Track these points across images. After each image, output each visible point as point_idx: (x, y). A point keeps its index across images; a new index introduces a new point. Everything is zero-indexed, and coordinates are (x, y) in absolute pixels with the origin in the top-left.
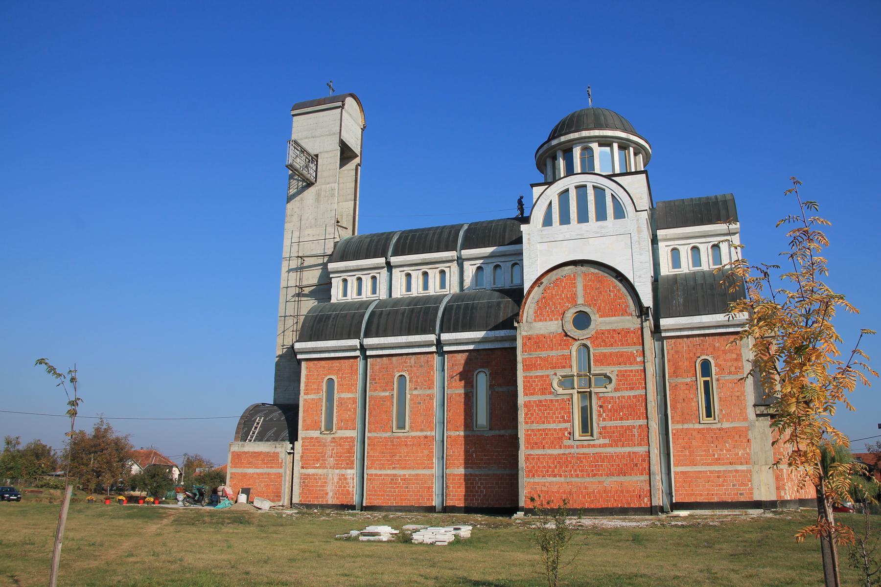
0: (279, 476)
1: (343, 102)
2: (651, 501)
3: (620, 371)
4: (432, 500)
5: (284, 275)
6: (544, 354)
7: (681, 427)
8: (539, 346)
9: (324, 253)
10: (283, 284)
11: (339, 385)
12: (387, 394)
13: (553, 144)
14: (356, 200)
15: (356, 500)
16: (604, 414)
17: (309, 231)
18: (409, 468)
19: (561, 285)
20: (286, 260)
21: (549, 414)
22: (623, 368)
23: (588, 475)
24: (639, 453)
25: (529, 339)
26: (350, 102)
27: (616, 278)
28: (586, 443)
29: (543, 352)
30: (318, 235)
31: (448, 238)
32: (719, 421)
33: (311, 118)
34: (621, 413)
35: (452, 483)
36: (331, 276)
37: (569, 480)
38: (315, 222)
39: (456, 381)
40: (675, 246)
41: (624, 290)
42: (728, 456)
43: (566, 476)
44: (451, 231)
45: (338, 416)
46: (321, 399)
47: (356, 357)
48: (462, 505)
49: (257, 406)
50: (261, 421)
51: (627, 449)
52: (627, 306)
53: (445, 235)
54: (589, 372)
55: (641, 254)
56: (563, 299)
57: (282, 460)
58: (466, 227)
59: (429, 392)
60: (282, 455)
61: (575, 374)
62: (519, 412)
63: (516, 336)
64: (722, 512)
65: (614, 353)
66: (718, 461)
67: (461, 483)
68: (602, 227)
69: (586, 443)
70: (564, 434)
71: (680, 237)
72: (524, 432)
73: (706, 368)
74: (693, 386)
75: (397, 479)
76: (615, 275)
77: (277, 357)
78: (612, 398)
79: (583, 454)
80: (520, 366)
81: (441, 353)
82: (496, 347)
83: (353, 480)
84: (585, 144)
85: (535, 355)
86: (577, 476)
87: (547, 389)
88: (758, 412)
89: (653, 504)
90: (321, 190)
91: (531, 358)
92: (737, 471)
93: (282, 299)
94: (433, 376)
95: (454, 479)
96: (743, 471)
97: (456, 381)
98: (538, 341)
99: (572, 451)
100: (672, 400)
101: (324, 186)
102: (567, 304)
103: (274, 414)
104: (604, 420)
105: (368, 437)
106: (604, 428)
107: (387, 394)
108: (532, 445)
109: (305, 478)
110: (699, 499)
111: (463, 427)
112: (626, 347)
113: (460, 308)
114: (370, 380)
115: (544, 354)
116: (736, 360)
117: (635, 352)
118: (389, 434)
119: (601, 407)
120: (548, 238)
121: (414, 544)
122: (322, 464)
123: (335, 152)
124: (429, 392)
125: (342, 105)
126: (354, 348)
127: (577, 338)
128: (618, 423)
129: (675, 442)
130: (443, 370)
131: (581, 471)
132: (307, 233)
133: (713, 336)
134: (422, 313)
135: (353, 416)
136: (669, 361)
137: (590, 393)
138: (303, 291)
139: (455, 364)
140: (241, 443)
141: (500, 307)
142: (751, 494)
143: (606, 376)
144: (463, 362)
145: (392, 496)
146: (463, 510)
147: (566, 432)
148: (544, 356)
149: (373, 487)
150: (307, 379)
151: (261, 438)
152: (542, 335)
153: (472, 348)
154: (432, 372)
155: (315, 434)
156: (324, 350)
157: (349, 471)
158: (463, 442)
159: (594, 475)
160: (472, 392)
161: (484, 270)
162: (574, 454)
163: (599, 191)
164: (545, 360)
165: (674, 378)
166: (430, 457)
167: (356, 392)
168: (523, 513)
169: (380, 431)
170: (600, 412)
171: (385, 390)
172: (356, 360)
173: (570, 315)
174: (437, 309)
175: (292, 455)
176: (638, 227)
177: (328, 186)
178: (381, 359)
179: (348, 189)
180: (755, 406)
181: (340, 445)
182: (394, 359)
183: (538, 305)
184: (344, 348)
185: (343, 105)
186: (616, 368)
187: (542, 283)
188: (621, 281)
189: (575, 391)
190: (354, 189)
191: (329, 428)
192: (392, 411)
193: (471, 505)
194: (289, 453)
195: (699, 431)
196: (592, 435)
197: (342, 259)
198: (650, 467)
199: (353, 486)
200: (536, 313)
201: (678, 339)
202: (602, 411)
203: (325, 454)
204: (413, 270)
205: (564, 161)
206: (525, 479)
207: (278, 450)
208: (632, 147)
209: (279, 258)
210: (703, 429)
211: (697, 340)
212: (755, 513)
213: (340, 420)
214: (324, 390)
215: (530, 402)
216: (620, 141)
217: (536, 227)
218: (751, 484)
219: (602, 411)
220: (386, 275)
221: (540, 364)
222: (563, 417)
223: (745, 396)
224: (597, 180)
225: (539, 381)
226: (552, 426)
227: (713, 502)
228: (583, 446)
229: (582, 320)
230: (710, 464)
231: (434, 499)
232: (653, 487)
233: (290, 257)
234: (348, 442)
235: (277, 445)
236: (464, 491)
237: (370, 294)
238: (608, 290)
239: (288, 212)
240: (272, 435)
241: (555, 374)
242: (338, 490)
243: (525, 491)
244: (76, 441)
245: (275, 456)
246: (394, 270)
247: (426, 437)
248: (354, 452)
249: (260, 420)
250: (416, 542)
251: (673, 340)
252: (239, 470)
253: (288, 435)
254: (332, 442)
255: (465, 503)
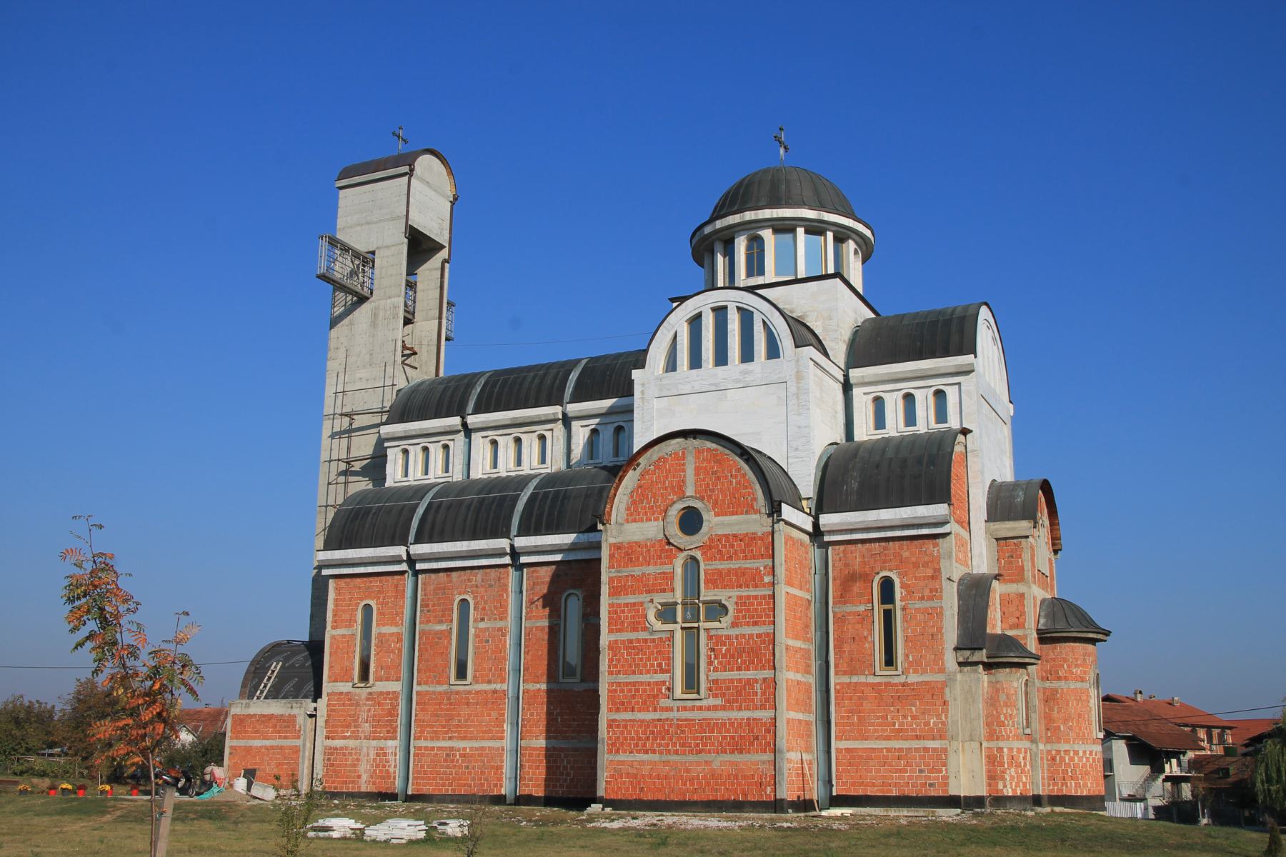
0: (296, 750)
1: (410, 165)
2: (775, 792)
3: (739, 597)
4: (501, 786)
5: (325, 441)
6: (637, 571)
7: (849, 681)
8: (631, 558)
9: (382, 408)
10: (324, 456)
11: (380, 614)
12: (444, 627)
13: (706, 233)
14: (442, 319)
15: (398, 785)
16: (716, 661)
17: (362, 373)
18: (471, 738)
19: (665, 467)
20: (329, 419)
21: (642, 659)
22: (745, 592)
23: (691, 752)
24: (762, 720)
25: (619, 548)
26: (426, 164)
27: (741, 456)
28: (689, 704)
29: (636, 569)
30: (374, 379)
31: (553, 383)
32: (903, 672)
33: (365, 193)
34: (739, 660)
35: (528, 761)
36: (386, 444)
37: (665, 758)
38: (370, 359)
39: (537, 607)
40: (878, 394)
41: (750, 475)
42: (914, 726)
43: (661, 753)
44: (558, 372)
45: (377, 660)
46: (354, 635)
47: (403, 573)
48: (541, 794)
49: (278, 645)
50: (278, 668)
51: (746, 714)
52: (754, 499)
53: (548, 380)
54: (699, 599)
55: (799, 414)
56: (666, 489)
57: (300, 727)
58: (584, 362)
59: (500, 624)
60: (301, 720)
61: (679, 601)
62: (601, 657)
63: (600, 541)
64: (899, 811)
65: (733, 569)
66: (899, 734)
67: (541, 761)
68: (746, 373)
69: (689, 704)
70: (661, 689)
71: (884, 379)
72: (607, 687)
73: (887, 589)
74: (865, 618)
75: (454, 755)
76: (739, 452)
77: (314, 569)
78: (728, 637)
79: (686, 720)
80: (605, 589)
81: (520, 567)
82: (593, 557)
83: (395, 755)
84: (752, 232)
85: (625, 572)
86: (676, 752)
87: (639, 623)
88: (961, 660)
89: (778, 797)
90: (379, 308)
91: (620, 577)
92: (926, 750)
93: (322, 481)
94: (506, 601)
95: (531, 755)
96: (935, 750)
97: (537, 607)
98: (630, 551)
99: (671, 715)
100: (839, 640)
101: (382, 302)
102: (671, 497)
103: (298, 657)
104: (716, 670)
105: (417, 692)
106: (715, 682)
107: (444, 627)
108: (617, 706)
109: (330, 752)
110: (870, 791)
111: (545, 677)
112: (749, 561)
113: (547, 497)
114: (421, 606)
115: (637, 571)
116: (933, 577)
117: (762, 568)
118: (444, 688)
119: (712, 650)
120: (668, 390)
121: (366, 841)
122: (354, 732)
123: (400, 247)
124: (500, 624)
125: (410, 170)
126: (398, 559)
127: (682, 547)
128: (735, 675)
129: (839, 704)
130: (521, 592)
131: (682, 745)
132: (358, 375)
133: (900, 541)
134: (495, 504)
135: (398, 661)
136: (834, 579)
137: (698, 628)
138: (353, 466)
139: (538, 583)
140: (245, 701)
141: (602, 496)
142: (946, 785)
143: (719, 603)
144: (548, 579)
145: (448, 779)
146: (543, 800)
147: (664, 688)
148: (638, 574)
149: (422, 767)
150: (336, 605)
151: (274, 694)
152: (636, 543)
153: (559, 559)
154: (505, 595)
155: (345, 687)
156: (357, 562)
157: (391, 743)
158: (546, 700)
159: (700, 752)
160: (558, 625)
161: (601, 435)
162: (673, 720)
163: (746, 316)
164: (639, 579)
165: (840, 605)
166: (499, 722)
167: (402, 625)
168: (601, 806)
169: (433, 683)
170: (711, 658)
171: (440, 622)
172: (402, 577)
173: (674, 512)
174: (515, 499)
175: (314, 719)
176: (797, 372)
177: (389, 301)
178: (437, 575)
179: (431, 299)
180: (956, 649)
181: (379, 704)
182: (454, 574)
183: (632, 497)
184: (385, 560)
185: (412, 170)
186: (735, 593)
187: (638, 465)
188: (747, 461)
189: (678, 626)
190: (438, 300)
191: (364, 676)
192: (450, 653)
193: (554, 795)
194: (311, 716)
195: (874, 685)
196: (698, 693)
197: (401, 420)
198: (775, 741)
199: (396, 770)
200: (629, 509)
201: (849, 546)
202: (713, 656)
203: (358, 718)
204: (501, 435)
205: (724, 257)
206: (606, 756)
207: (295, 711)
208: (830, 230)
209: (321, 417)
210: (880, 684)
211: (877, 546)
212: (948, 815)
213: (380, 666)
214: (359, 622)
215: (616, 641)
216: (808, 223)
217: (653, 373)
218: (946, 770)
219: (713, 656)
220: (463, 444)
221: (632, 586)
222: (660, 665)
223: (942, 635)
224: (742, 298)
225: (630, 611)
226: (644, 678)
227: (890, 796)
228: (685, 709)
229: (691, 522)
230: (888, 738)
231: (504, 784)
232: (779, 771)
233: (334, 414)
234: (391, 699)
235: (294, 705)
236: (544, 773)
237: (440, 473)
238: (729, 474)
239: (332, 344)
240: (292, 689)
241: (652, 601)
242: (375, 771)
243: (606, 774)
244: (81, 697)
245: (291, 720)
246: (474, 436)
247: (495, 692)
248: (398, 714)
249: (276, 666)
250: (368, 839)
251: (842, 548)
252: (242, 743)
253: (312, 689)
254: (368, 699)
255: (545, 790)
